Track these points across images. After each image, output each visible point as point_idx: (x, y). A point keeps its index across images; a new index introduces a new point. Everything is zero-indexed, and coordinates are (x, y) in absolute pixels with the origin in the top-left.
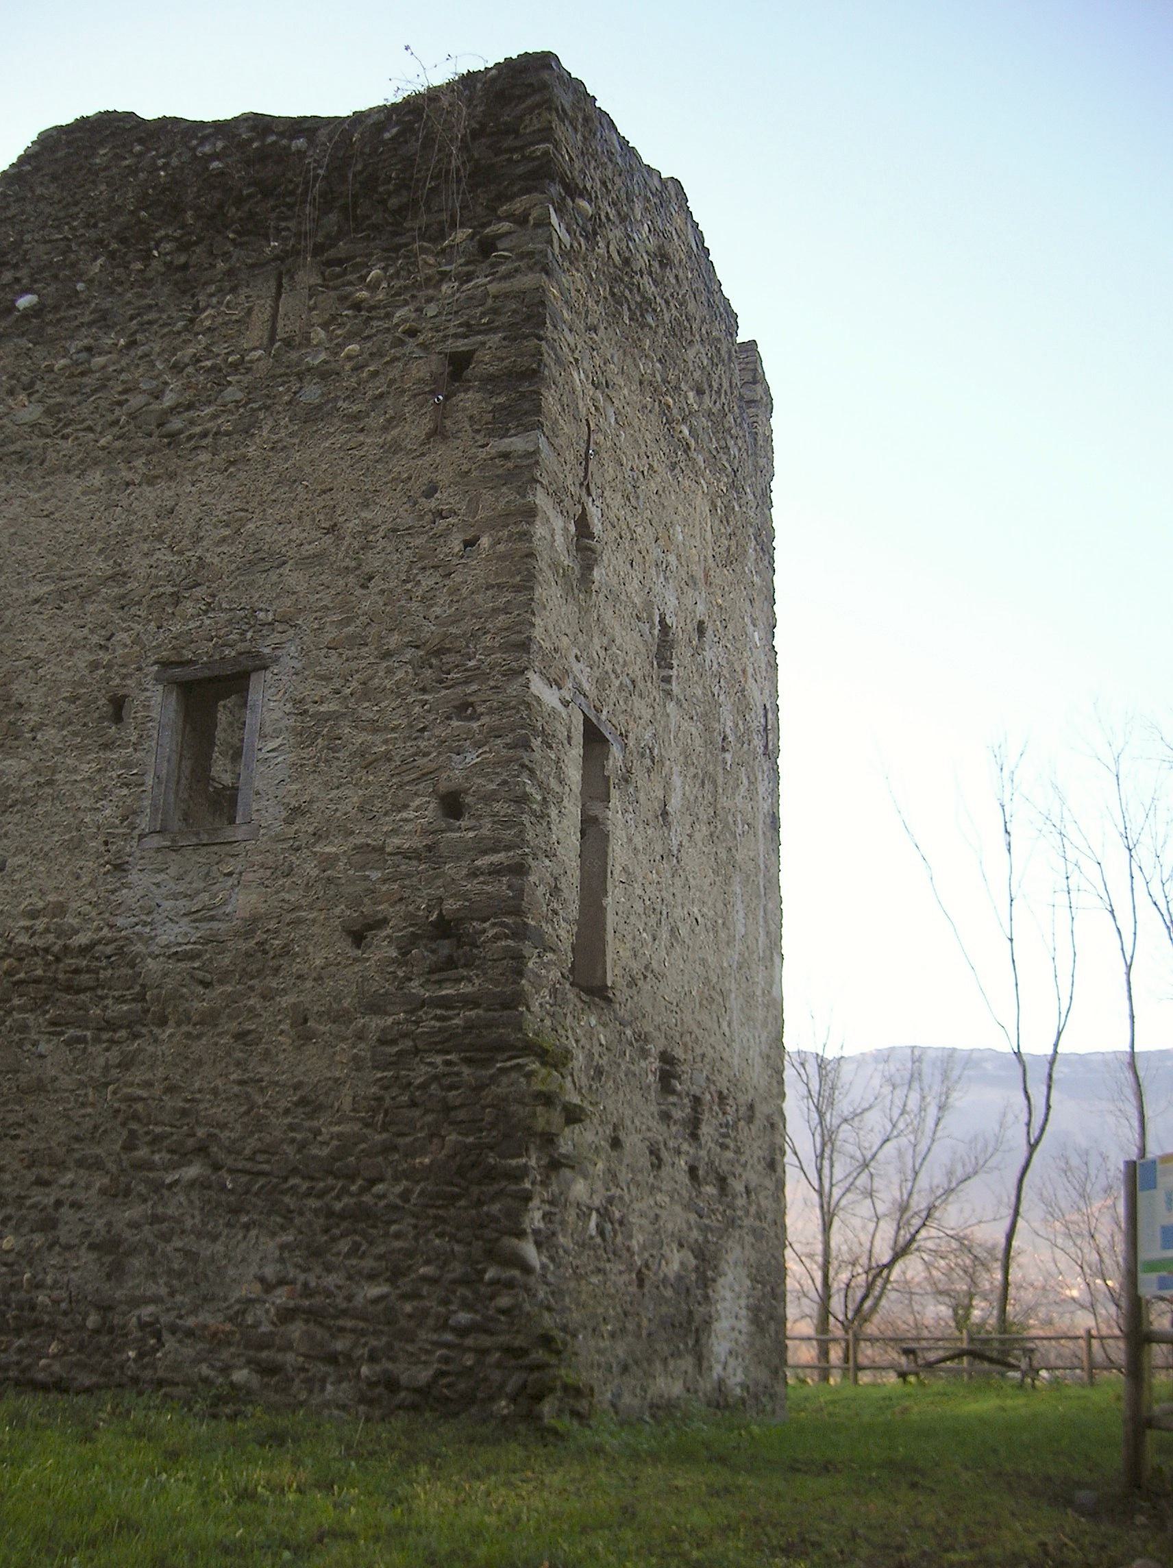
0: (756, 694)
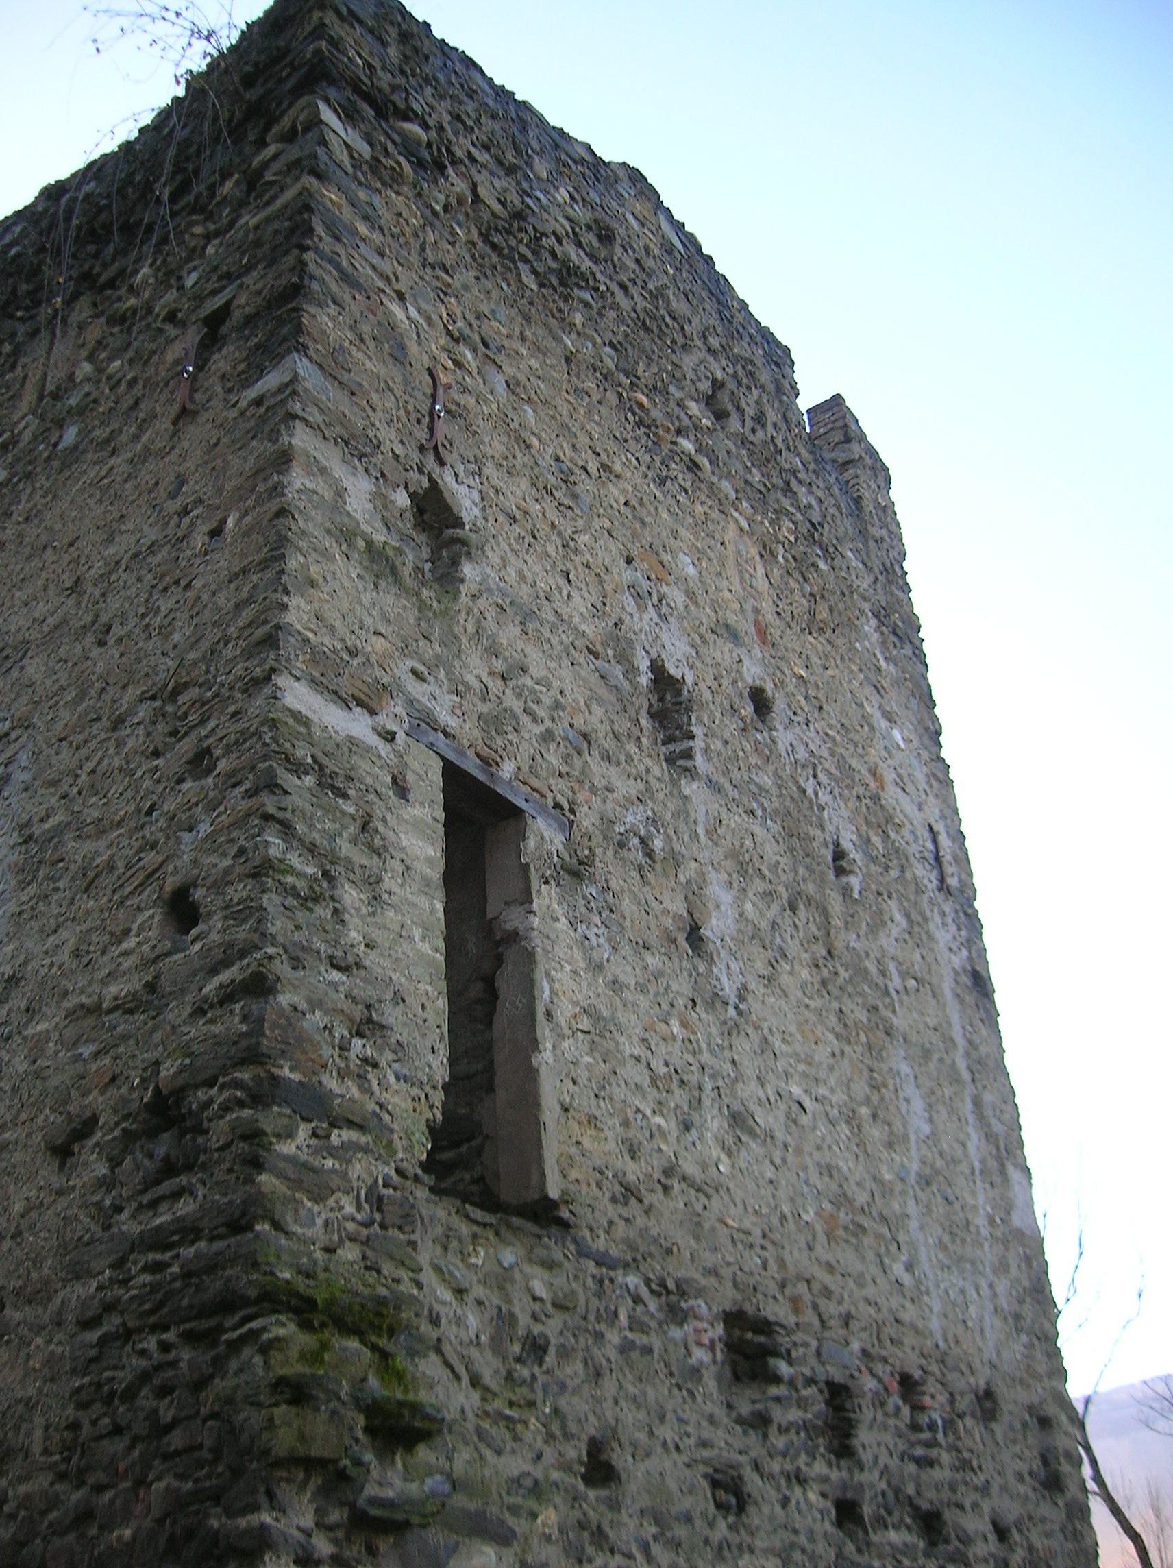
0: (911, 809)
